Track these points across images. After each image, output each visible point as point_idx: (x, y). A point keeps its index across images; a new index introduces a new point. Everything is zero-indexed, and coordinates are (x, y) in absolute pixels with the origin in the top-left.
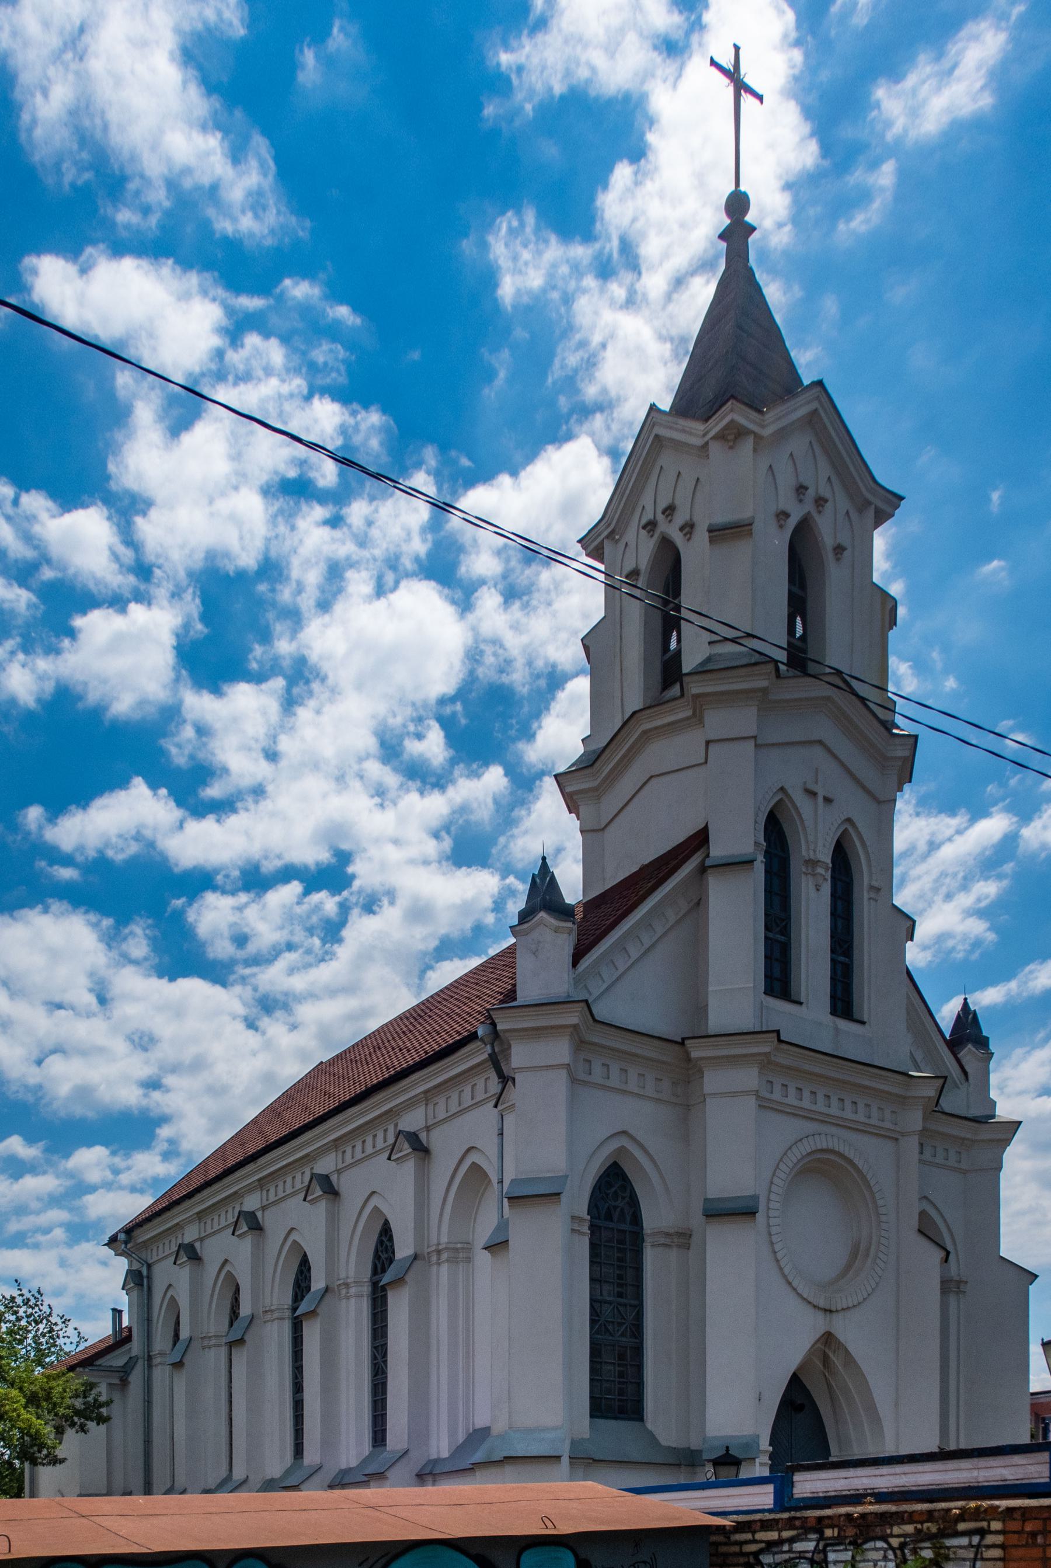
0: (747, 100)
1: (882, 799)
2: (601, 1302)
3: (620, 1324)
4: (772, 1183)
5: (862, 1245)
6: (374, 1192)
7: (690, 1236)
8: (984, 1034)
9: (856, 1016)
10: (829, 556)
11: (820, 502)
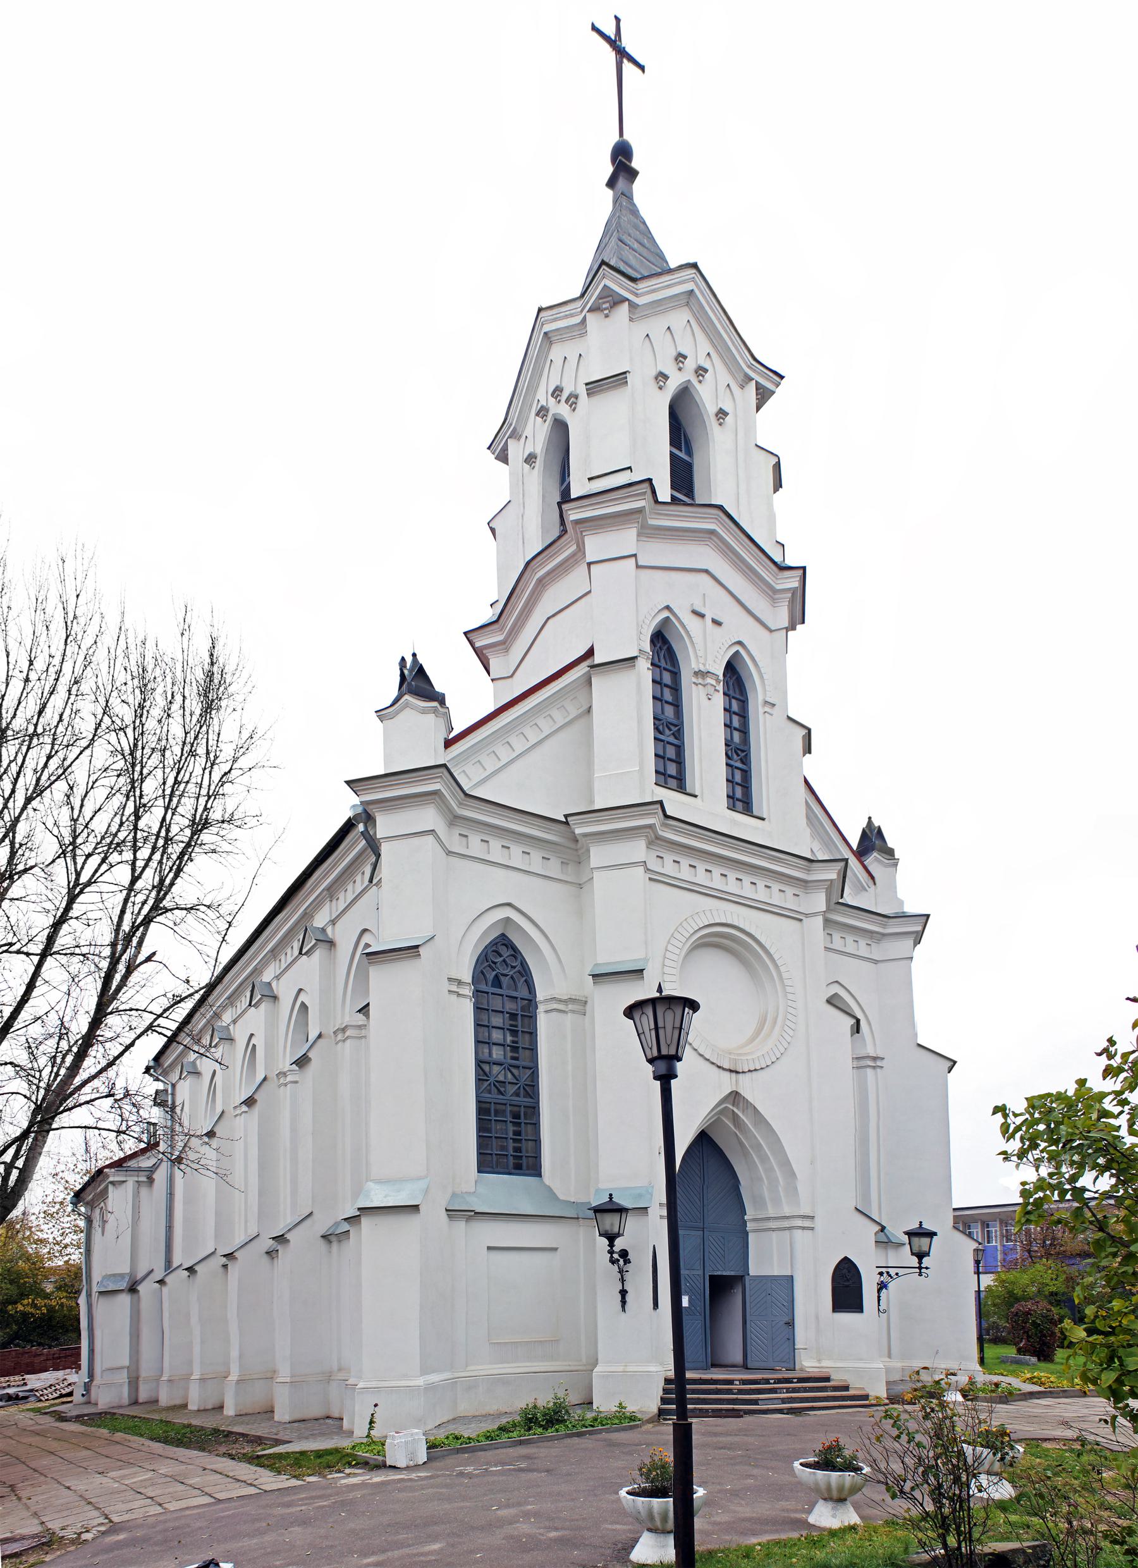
0: (627, 66)
2: (489, 1063)
5: (769, 1016)
6: (365, 930)
7: (586, 1002)
9: (755, 813)
10: (711, 422)
11: (701, 371)
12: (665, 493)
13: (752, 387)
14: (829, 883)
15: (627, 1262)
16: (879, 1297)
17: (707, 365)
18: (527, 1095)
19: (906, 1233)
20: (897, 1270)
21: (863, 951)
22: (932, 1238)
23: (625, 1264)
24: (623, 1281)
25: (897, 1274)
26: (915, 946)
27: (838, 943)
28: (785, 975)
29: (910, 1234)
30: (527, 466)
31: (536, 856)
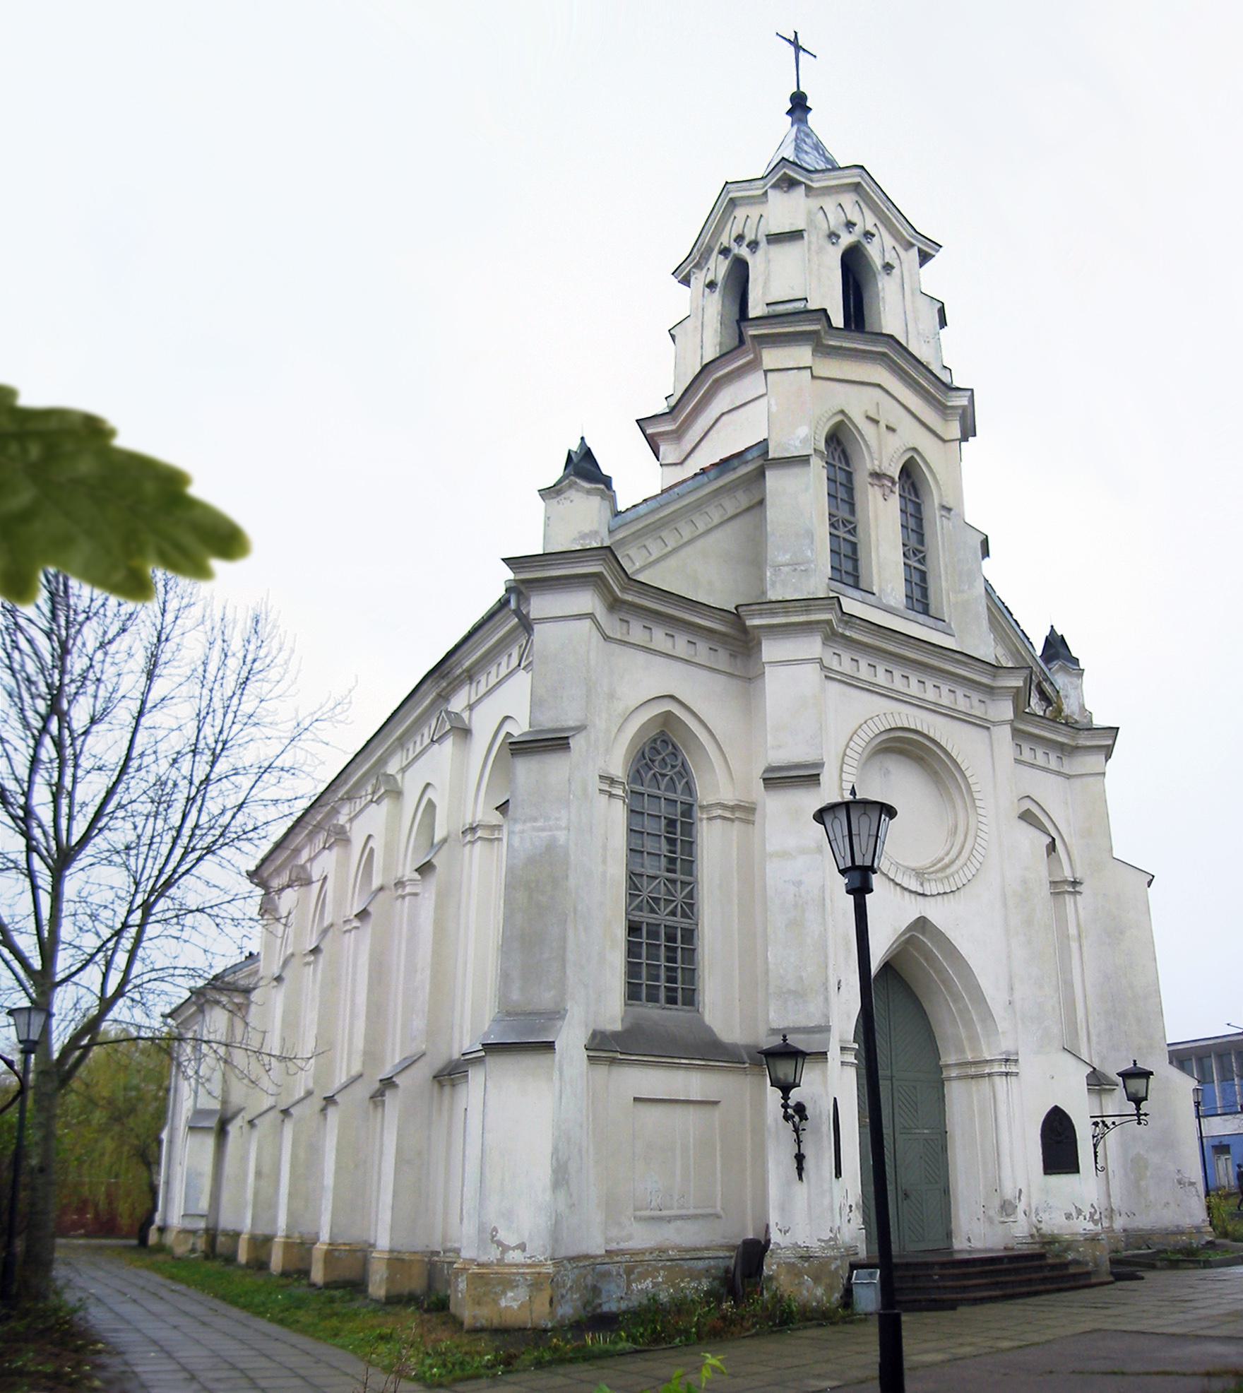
1: (946, 438)
3: (668, 902)
4: (845, 754)
6: (507, 718)
8: (605, 472)
9: (932, 612)
11: (868, 235)
12: (838, 320)
13: (915, 251)
14: (1015, 690)
15: (804, 1117)
16: (1096, 1153)
17: (874, 230)
18: (684, 915)
19: (1119, 1074)
20: (1113, 1119)
21: (1053, 763)
22: (1148, 1078)
23: (801, 1120)
24: (799, 1142)
25: (1114, 1123)
26: (1107, 761)
27: (1027, 755)
28: (974, 788)
29: (1125, 1075)
30: (707, 290)
31: (702, 646)
